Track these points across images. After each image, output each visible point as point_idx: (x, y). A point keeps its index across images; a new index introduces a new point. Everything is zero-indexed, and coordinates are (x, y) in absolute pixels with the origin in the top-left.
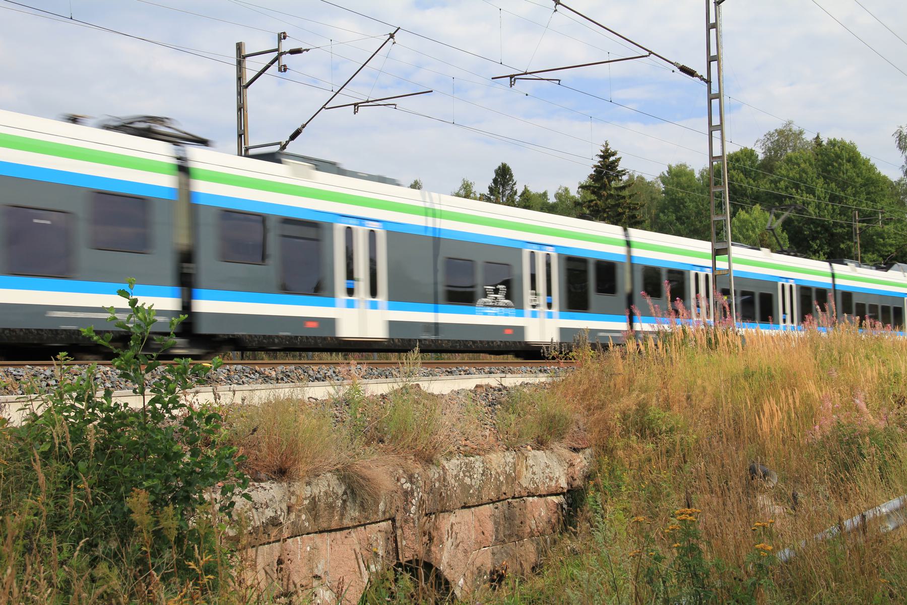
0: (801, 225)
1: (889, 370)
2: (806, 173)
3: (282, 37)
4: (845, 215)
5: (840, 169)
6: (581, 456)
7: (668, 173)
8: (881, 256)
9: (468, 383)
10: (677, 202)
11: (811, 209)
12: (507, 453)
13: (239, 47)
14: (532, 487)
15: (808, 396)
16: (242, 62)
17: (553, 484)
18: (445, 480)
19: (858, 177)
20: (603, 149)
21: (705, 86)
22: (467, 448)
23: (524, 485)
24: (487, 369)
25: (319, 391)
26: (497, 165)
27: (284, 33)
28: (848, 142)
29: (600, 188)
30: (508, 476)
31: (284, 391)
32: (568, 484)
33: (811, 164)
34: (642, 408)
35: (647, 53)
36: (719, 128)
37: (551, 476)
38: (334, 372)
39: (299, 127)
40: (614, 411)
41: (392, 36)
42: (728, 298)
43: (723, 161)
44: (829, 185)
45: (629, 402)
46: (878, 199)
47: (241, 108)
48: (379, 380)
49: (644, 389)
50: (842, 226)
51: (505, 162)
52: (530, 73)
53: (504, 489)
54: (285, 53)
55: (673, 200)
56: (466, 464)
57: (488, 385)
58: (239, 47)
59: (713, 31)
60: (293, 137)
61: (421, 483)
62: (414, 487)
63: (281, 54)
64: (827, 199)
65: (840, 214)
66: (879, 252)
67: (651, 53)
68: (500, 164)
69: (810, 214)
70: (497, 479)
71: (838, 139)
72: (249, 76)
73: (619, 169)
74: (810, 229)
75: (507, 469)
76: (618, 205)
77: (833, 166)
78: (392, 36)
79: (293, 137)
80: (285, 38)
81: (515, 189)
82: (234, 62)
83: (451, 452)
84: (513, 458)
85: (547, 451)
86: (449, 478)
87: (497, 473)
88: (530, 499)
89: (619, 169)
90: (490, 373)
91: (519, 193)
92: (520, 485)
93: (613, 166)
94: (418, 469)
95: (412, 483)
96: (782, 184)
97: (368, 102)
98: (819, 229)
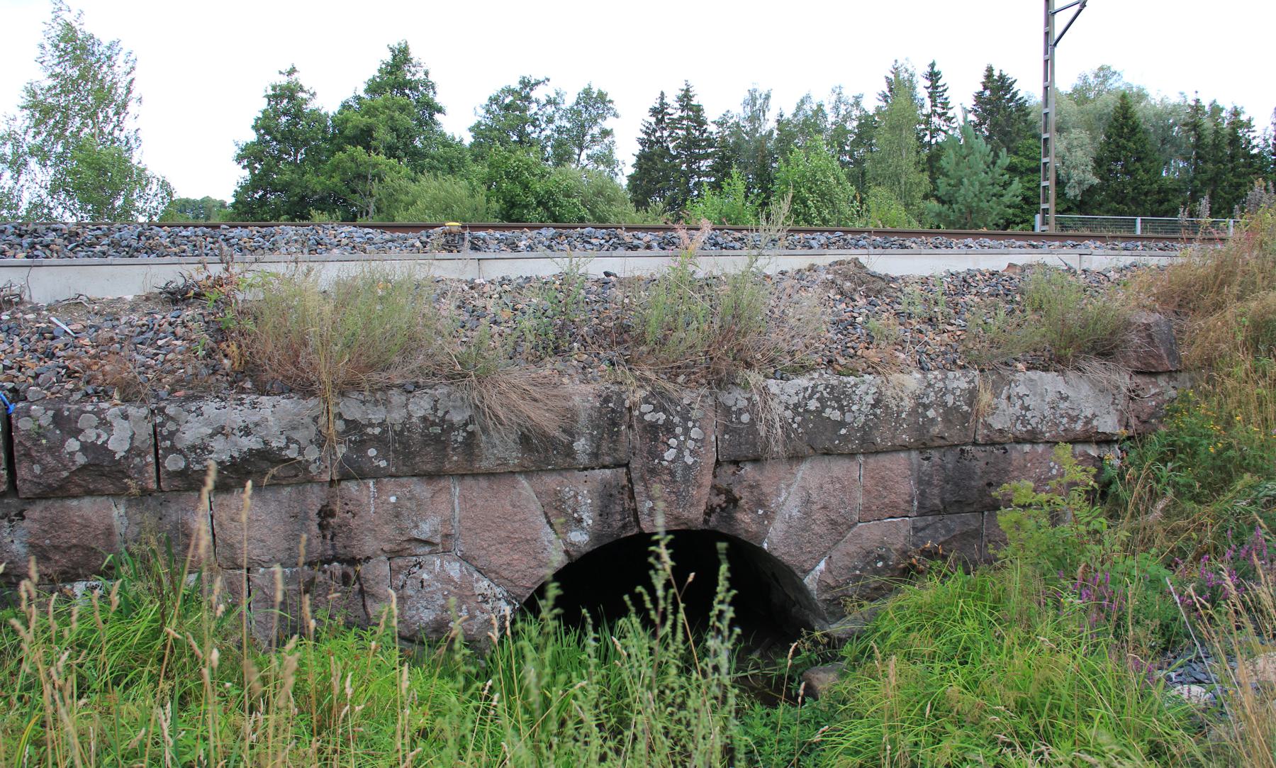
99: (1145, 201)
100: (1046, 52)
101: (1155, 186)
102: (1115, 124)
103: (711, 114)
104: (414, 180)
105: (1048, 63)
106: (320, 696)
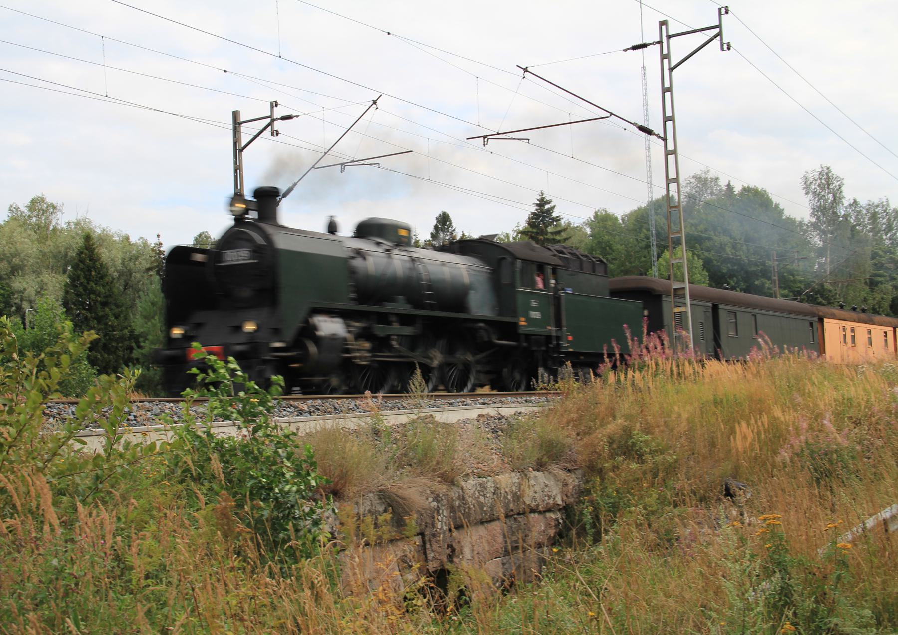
1: (843, 395)
3: (274, 105)
6: (573, 476)
8: (793, 292)
12: (513, 474)
13: (236, 115)
14: (533, 504)
15: (775, 418)
17: (551, 501)
18: (464, 499)
20: (539, 198)
21: (662, 142)
24: (481, 401)
26: (438, 213)
27: (276, 102)
29: (537, 234)
31: (330, 423)
32: (563, 501)
35: (608, 115)
37: (550, 494)
38: (356, 405)
41: (375, 102)
43: (679, 210)
45: (613, 427)
48: (393, 412)
49: (627, 417)
53: (511, 506)
54: (277, 119)
55: (599, 243)
56: (481, 485)
57: (488, 414)
58: (236, 115)
59: (667, 95)
62: (439, 505)
63: (273, 120)
66: (790, 288)
67: (612, 114)
68: (440, 213)
70: (505, 498)
75: (514, 488)
80: (276, 105)
83: (468, 475)
85: (545, 472)
86: (467, 497)
87: (506, 492)
88: (532, 515)
89: (554, 215)
92: (524, 503)
93: (549, 211)
94: (442, 489)
95: (438, 502)
99: (117, 348)
100: (235, 157)
101: (126, 331)
102: (81, 266)
103: (848, 196)
104: (667, 601)
105: (238, 168)
106: (827, 174)
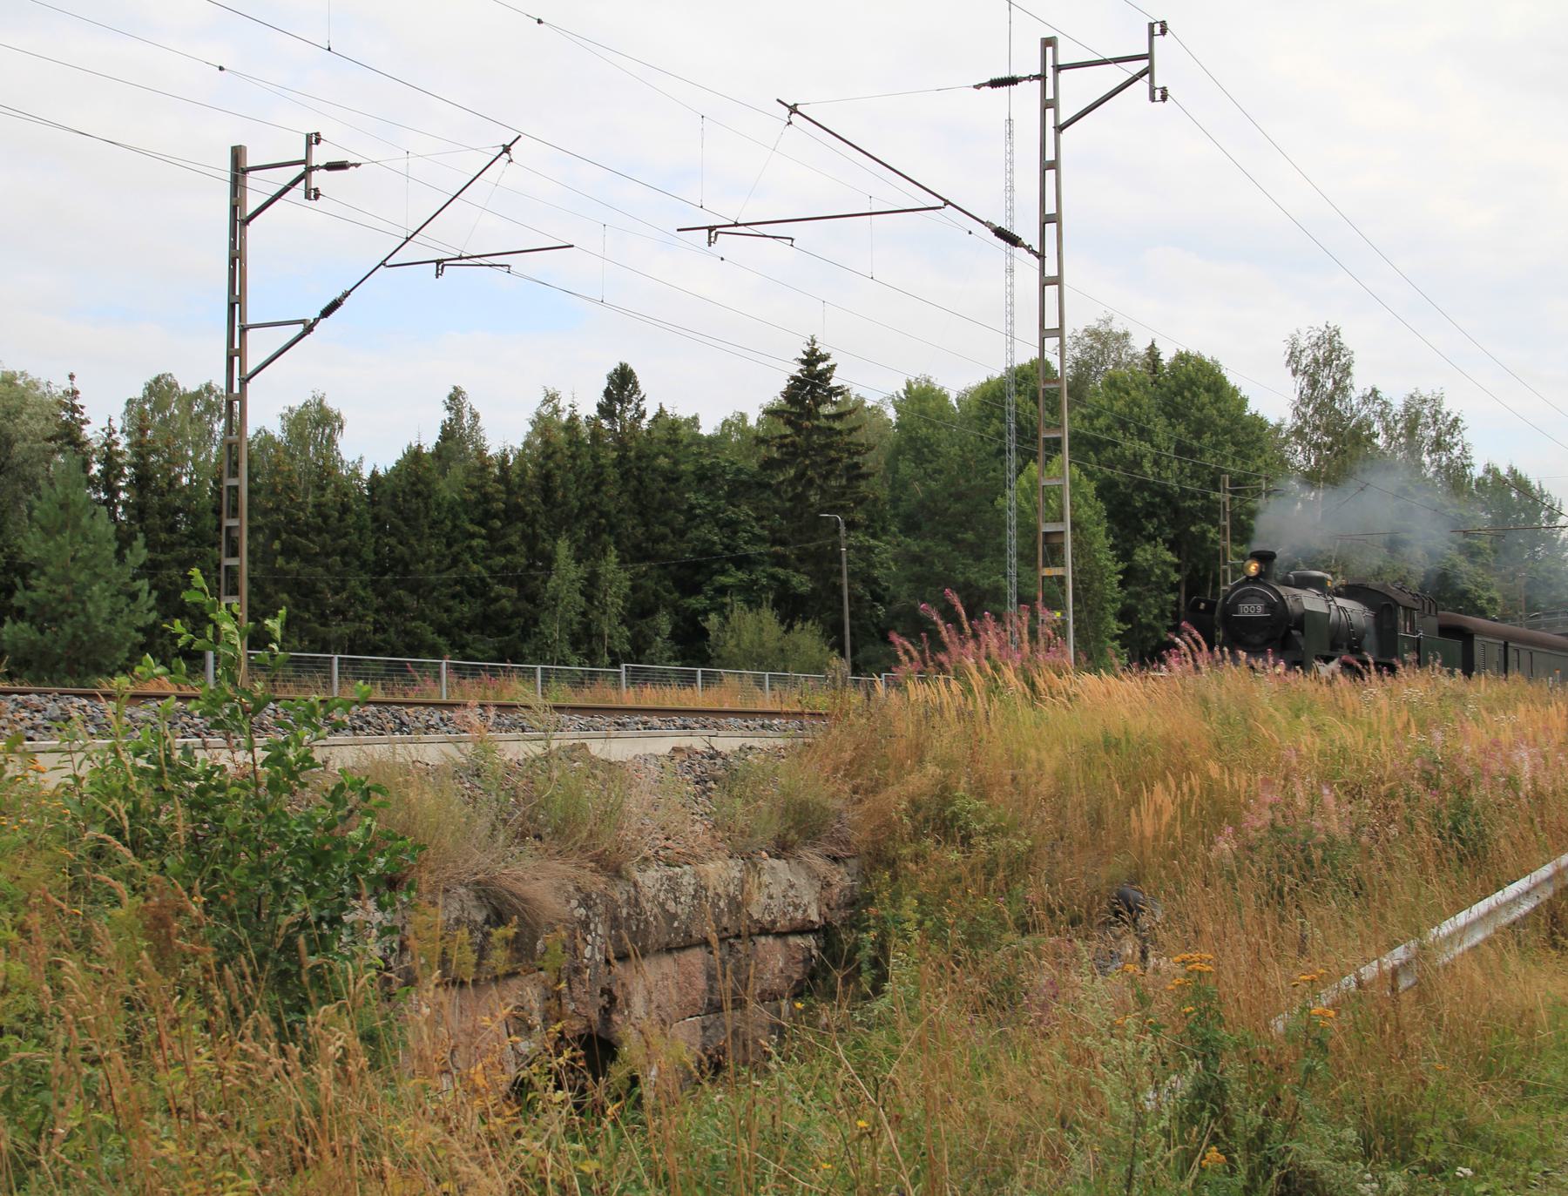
0: (1129, 491)
2: (1140, 407)
3: (313, 139)
4: (1198, 478)
5: (1192, 401)
7: (905, 392)
9: (662, 745)
10: (919, 443)
11: (1147, 465)
12: (731, 862)
13: (237, 154)
16: (240, 179)
19: (1222, 416)
20: (807, 349)
21: (1037, 261)
22: (669, 851)
23: (756, 916)
24: (679, 722)
25: (432, 751)
27: (317, 134)
28: (1207, 358)
30: (732, 900)
33: (1146, 392)
34: (944, 793)
35: (941, 203)
36: (1057, 333)
39: (338, 295)
40: (895, 797)
41: (507, 149)
42: (1063, 614)
44: (1174, 428)
45: (922, 780)
46: (1253, 453)
47: (237, 256)
50: (1193, 497)
51: (624, 361)
52: (745, 225)
54: (318, 168)
55: (911, 439)
56: (670, 879)
57: (689, 748)
58: (237, 154)
60: (327, 312)
61: (601, 908)
63: (310, 169)
64: (1172, 450)
65: (1191, 478)
67: (947, 203)
68: (617, 366)
69: (1145, 474)
71: (1193, 352)
72: (252, 203)
73: (833, 383)
74: (1143, 499)
75: (731, 888)
76: (829, 446)
77: (1183, 397)
78: (507, 149)
79: (327, 312)
80: (318, 142)
81: (642, 408)
82: (228, 177)
83: (646, 859)
84: (740, 871)
88: (763, 940)
89: (833, 383)
90: (685, 728)
91: (650, 416)
93: (824, 376)
95: (589, 908)
96: (1101, 422)
97: (460, 258)
98: (1157, 500)
